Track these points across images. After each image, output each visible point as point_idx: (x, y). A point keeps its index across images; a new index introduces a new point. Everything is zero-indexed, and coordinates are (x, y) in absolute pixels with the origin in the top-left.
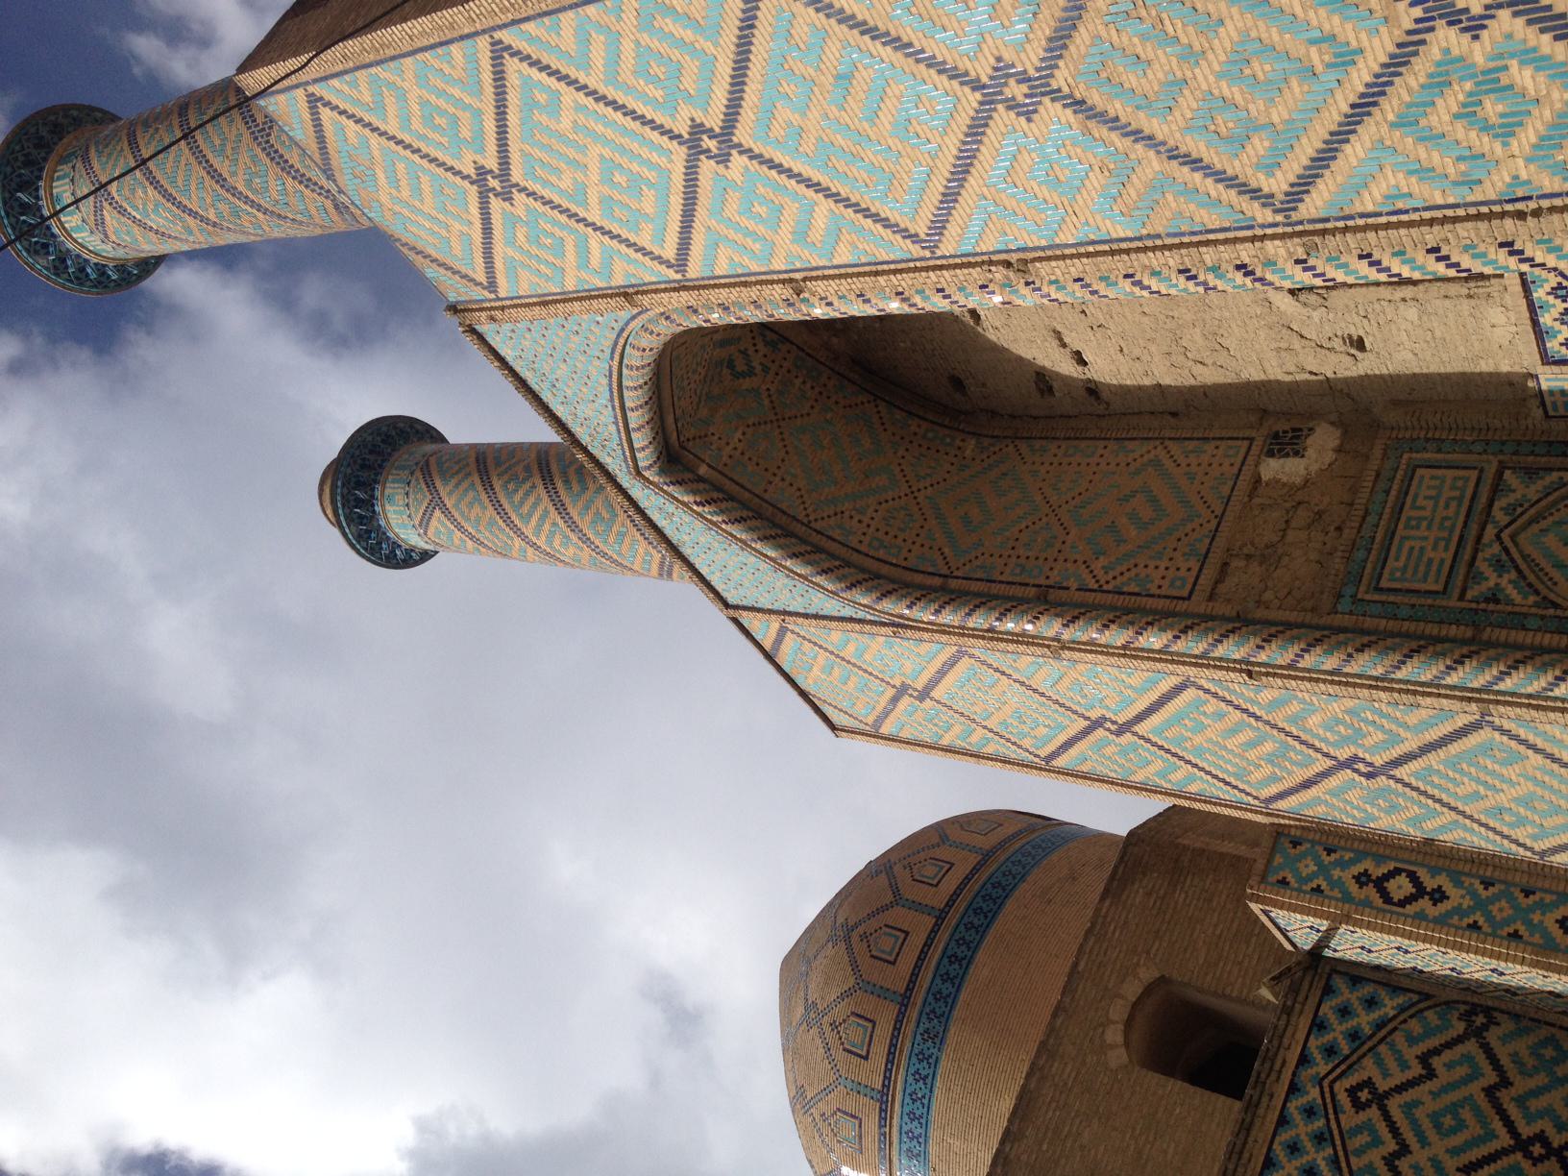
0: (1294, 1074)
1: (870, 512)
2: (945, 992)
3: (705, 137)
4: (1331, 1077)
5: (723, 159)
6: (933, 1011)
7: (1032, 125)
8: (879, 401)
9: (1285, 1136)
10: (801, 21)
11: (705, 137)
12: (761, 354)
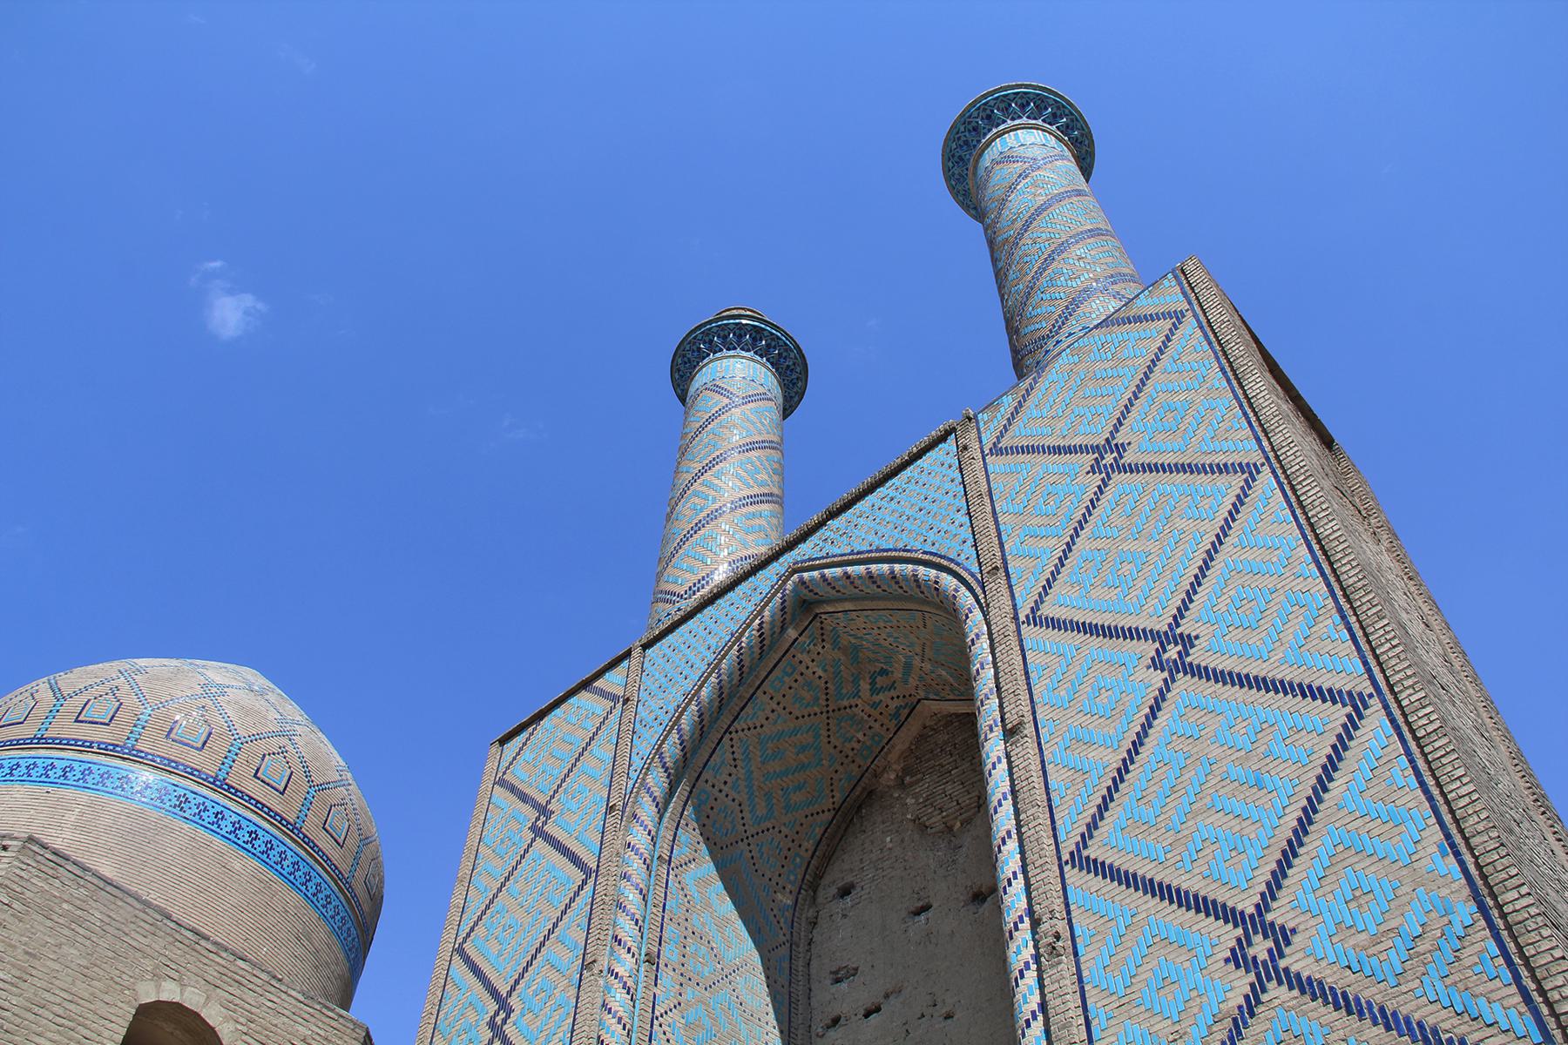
1: (733, 794)
2: (222, 823)
5: (1157, 663)
6: (206, 809)
7: (1223, 963)
8: (833, 812)
10: (1315, 741)
12: (889, 702)
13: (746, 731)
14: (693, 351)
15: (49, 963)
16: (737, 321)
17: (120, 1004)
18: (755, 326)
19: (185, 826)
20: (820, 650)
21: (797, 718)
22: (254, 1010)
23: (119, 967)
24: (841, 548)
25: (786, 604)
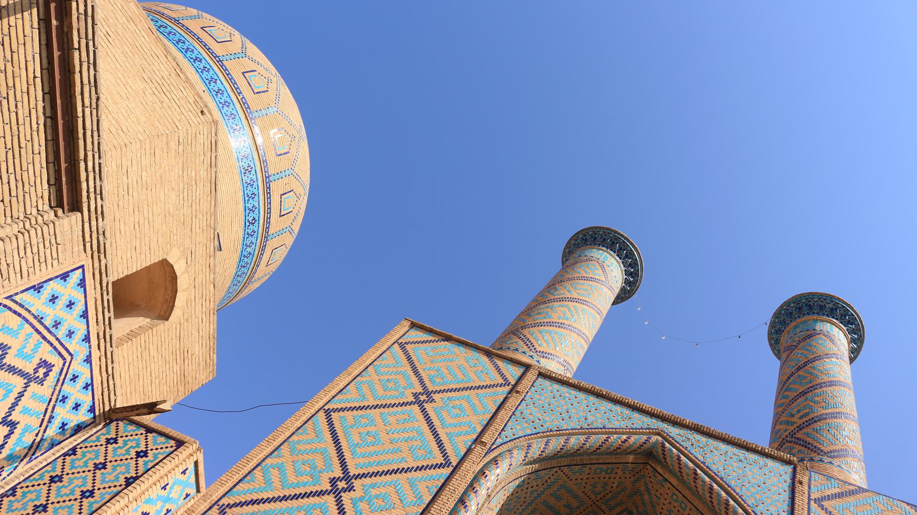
0: (90, 347)
3: (420, 396)
4: (67, 364)
5: (416, 395)
9: (79, 308)
11: (420, 396)
13: (564, 475)
14: (592, 237)
15: (162, 193)
16: (633, 249)
17: (161, 248)
18: (636, 260)
19: (239, 183)
20: (628, 477)
21: (584, 492)
22: (193, 317)
23: (178, 229)
24: (698, 454)
25: (644, 445)
